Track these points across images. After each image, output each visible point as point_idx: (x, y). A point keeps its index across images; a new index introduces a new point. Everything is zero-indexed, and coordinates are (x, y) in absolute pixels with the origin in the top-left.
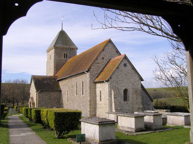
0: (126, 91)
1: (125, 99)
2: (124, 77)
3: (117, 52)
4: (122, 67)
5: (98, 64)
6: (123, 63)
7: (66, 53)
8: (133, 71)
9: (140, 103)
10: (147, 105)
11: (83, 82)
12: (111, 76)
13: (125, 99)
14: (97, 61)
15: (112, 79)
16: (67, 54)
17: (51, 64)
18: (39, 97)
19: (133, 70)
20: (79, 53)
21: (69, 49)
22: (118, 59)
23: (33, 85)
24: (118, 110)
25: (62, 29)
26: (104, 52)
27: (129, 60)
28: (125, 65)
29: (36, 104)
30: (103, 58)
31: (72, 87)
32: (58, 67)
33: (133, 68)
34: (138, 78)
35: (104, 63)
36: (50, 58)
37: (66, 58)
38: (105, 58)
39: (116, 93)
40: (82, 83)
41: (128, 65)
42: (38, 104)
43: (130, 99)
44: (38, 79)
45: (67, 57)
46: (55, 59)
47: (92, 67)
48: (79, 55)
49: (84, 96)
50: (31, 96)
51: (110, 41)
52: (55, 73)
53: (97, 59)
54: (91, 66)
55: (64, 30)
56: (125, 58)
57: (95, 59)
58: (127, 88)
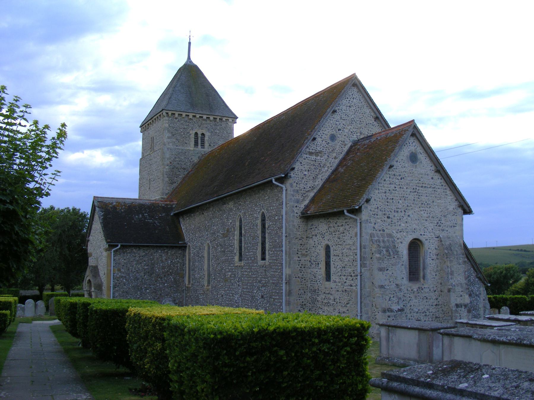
0: (415, 246)
3: (376, 118)
8: (438, 180)
9: (462, 287)
11: (263, 216)
13: (414, 272)
19: (437, 176)
23: (97, 227)
24: (392, 311)
29: (104, 288)
30: (333, 138)
31: (224, 236)
35: (334, 155)
38: (340, 138)
39: (387, 251)
40: (259, 222)
42: (114, 287)
43: (429, 276)
44: (114, 207)
50: (92, 262)
55: (195, 60)
58: (421, 238)
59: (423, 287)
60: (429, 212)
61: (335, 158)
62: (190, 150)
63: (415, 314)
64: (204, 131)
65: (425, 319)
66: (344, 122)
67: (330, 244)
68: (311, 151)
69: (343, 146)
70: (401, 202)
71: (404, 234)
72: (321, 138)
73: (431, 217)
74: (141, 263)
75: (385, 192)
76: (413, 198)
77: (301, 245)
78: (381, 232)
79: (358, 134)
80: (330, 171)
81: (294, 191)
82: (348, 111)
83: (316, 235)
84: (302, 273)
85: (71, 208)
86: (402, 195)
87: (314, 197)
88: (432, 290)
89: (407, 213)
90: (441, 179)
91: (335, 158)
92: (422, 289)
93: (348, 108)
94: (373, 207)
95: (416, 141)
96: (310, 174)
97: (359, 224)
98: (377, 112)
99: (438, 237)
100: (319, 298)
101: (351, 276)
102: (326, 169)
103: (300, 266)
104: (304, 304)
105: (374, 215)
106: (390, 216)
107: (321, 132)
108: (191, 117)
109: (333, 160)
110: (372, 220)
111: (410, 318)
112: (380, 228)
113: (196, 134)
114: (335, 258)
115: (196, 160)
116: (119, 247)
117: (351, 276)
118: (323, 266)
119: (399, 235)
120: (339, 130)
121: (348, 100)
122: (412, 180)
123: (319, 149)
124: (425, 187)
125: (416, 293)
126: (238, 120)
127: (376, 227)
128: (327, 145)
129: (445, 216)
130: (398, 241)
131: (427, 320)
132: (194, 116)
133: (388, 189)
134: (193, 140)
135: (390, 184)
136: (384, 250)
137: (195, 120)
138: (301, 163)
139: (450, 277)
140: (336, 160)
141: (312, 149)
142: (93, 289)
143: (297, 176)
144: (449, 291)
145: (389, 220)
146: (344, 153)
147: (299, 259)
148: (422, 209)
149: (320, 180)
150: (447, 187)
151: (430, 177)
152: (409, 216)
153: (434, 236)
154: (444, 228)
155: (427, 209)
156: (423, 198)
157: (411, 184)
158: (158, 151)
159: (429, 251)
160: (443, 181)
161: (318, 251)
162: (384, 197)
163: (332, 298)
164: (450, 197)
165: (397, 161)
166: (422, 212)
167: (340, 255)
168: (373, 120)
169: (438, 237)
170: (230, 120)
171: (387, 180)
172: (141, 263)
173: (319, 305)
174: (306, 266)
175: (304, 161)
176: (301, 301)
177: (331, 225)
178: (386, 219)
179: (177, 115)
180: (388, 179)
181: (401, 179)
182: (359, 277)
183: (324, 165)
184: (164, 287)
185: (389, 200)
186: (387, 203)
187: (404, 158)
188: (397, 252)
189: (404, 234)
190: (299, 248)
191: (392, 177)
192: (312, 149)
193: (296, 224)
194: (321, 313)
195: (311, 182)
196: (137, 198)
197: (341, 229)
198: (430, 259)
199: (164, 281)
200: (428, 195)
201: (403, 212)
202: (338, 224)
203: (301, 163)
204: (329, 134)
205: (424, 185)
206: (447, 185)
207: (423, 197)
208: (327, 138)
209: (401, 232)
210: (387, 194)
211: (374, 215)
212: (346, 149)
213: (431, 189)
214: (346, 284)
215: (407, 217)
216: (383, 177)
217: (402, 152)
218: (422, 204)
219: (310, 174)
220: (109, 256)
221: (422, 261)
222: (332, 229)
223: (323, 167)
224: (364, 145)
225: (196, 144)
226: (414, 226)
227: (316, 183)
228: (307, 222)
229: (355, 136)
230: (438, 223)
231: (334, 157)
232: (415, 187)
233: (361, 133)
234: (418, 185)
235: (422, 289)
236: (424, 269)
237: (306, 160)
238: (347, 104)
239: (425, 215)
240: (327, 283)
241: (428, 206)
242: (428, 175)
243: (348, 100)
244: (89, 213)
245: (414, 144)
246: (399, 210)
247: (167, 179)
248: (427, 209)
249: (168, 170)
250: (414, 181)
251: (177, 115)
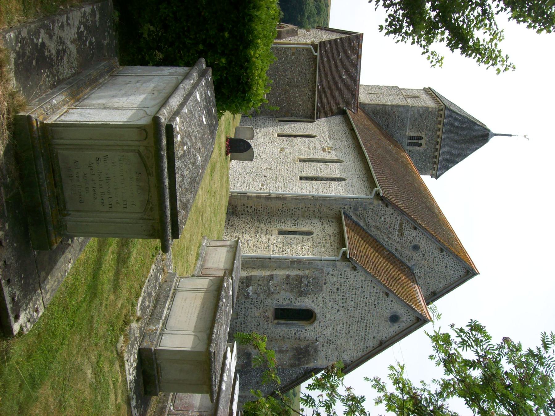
0: (307, 316)
1: (284, 314)
2: (357, 314)
5: (400, 231)
6: (400, 310)
8: (372, 344)
10: (258, 383)
13: (284, 314)
14: (407, 227)
16: (420, 145)
17: (391, 98)
20: (427, 179)
21: (436, 154)
22: (414, 299)
25: (496, 135)
26: (436, 253)
28: (394, 319)
30: (416, 248)
35: (399, 248)
36: (409, 97)
37: (409, 141)
38: (416, 256)
41: (395, 328)
45: (410, 144)
46: (406, 108)
47: (389, 210)
50: (301, 31)
51: (469, 272)
52: (364, 107)
53: (415, 229)
54: (396, 207)
55: (492, 141)
56: (418, 319)
57: (415, 221)
59: (269, 322)
60: (342, 332)
61: (396, 249)
62: (406, 132)
63: (243, 313)
64: (423, 146)
65: (238, 323)
66: (431, 260)
67: (314, 235)
68: (404, 225)
69: (407, 258)
70: (352, 303)
71: (321, 305)
72: (416, 236)
73: (336, 334)
74: (299, 75)
75: (362, 287)
76: (355, 316)
77: (314, 211)
78: (324, 281)
79: (419, 274)
82: (442, 265)
83: (322, 225)
84: (287, 212)
86: (359, 305)
87: (360, 226)
88: (265, 331)
89: (341, 308)
90: (373, 347)
91: (396, 249)
92: (267, 321)
93: (445, 265)
94: (349, 274)
95: (411, 323)
96: (382, 222)
98: (440, 294)
99: (316, 340)
100: (262, 225)
102: (386, 240)
103: (294, 210)
104: (258, 212)
105: (341, 275)
106: (339, 291)
107: (422, 236)
108: (438, 133)
109: (395, 247)
110: (336, 273)
111: (240, 308)
112: (328, 280)
113: (421, 138)
114: (301, 239)
116: (315, 54)
117: (283, 251)
118: (293, 229)
119: (320, 299)
120: (424, 255)
121: (453, 265)
122: (373, 316)
123: (406, 233)
124: (366, 329)
125: (264, 314)
126: (434, 179)
128: (409, 242)
130: (315, 298)
131: (237, 325)
133: (365, 290)
135: (370, 293)
137: (434, 137)
138: (392, 214)
140: (394, 250)
141: (405, 226)
143: (380, 210)
145: (335, 291)
146: (401, 258)
147: (300, 208)
148: (345, 325)
150: (365, 353)
151: (375, 335)
152: (339, 311)
153: (318, 336)
154: (325, 347)
155: (344, 330)
156: (355, 326)
157: (369, 315)
158: (405, 101)
159: (304, 331)
160: (372, 349)
161: (307, 226)
162: (358, 286)
164: (355, 356)
165: (392, 301)
166: (341, 325)
168: (433, 291)
169: (316, 340)
170: (434, 172)
171: (375, 289)
172: (299, 75)
174: (293, 216)
175: (395, 217)
176: (260, 209)
177: (332, 237)
178: (336, 287)
179: (440, 119)
180: (375, 291)
181: (375, 305)
183: (390, 238)
184: (277, 98)
185: (354, 290)
186: (351, 288)
187: (395, 309)
189: (321, 305)
190: (311, 209)
191: (377, 295)
192: (405, 226)
194: (249, 226)
195: (374, 224)
196: (360, 84)
197: (328, 245)
198: (296, 331)
199: (282, 97)
200: (358, 332)
201: (342, 305)
203: (392, 214)
204: (419, 244)
205: (368, 328)
206: (368, 352)
207: (356, 326)
208: (416, 242)
209: (323, 301)
210: (360, 289)
211: (341, 275)
213: (363, 335)
215: (338, 308)
216: (377, 286)
217: (401, 307)
218: (350, 325)
219: (382, 222)
221: (294, 322)
222: (328, 238)
223: (388, 237)
225: (411, 138)
226: (328, 316)
227: (373, 229)
228: (336, 218)
229: (417, 271)
230: (330, 341)
231: (398, 248)
233: (419, 277)
234: (369, 321)
235: (267, 321)
237: (395, 220)
238: (447, 266)
239: (339, 328)
240: (277, 232)
241: (347, 332)
242: (378, 333)
243: (453, 265)
245: (408, 320)
246: (344, 301)
248: (344, 330)
249: (387, 109)
250: (372, 318)
251: (440, 119)
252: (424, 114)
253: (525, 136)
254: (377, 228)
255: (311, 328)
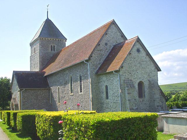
0: (141, 84)
2: (138, 65)
3: (122, 36)
4: (135, 53)
7: (53, 45)
12: (123, 63)
13: (141, 94)
15: (124, 69)
18: (23, 96)
19: (147, 57)
20: (68, 44)
23: (15, 82)
26: (107, 36)
27: (142, 44)
28: (138, 51)
29: (19, 105)
30: (106, 44)
32: (47, 60)
33: (148, 54)
34: (153, 68)
35: (107, 51)
38: (109, 44)
41: (141, 50)
47: (93, 55)
48: (71, 45)
49: (82, 93)
50: (13, 96)
51: (113, 23)
53: (99, 45)
54: (92, 53)
55: (50, 18)
56: (138, 41)
58: (143, 81)
67: (107, 84)
79: (116, 43)
80: (106, 57)
81: (92, 65)
85: (4, 78)
91: (107, 52)
97: (119, 76)
100: (104, 106)
101: (117, 97)
110: (124, 75)
113: (9, 114)
115: (52, 56)
117: (117, 97)
118: (105, 93)
127: (126, 77)
129: (151, 72)
132: (50, 39)
134: (50, 48)
136: (129, 86)
139: (154, 95)
142: (14, 107)
144: (154, 101)
146: (110, 50)
149: (102, 60)
156: (143, 66)
160: (149, 59)
163: (109, 105)
166: (143, 71)
167: (112, 89)
173: (104, 108)
182: (120, 97)
185: (130, 67)
188: (134, 87)
193: (93, 77)
196: (30, 71)
202: (111, 77)
212: (111, 48)
214: (115, 100)
220: (20, 94)
221: (143, 89)
224: (119, 46)
225: (52, 50)
232: (139, 62)
236: (144, 93)
244: (11, 80)
247: (41, 63)
252: (42, 46)
253: (48, 6)
254: (100, 60)
255: (145, 83)
